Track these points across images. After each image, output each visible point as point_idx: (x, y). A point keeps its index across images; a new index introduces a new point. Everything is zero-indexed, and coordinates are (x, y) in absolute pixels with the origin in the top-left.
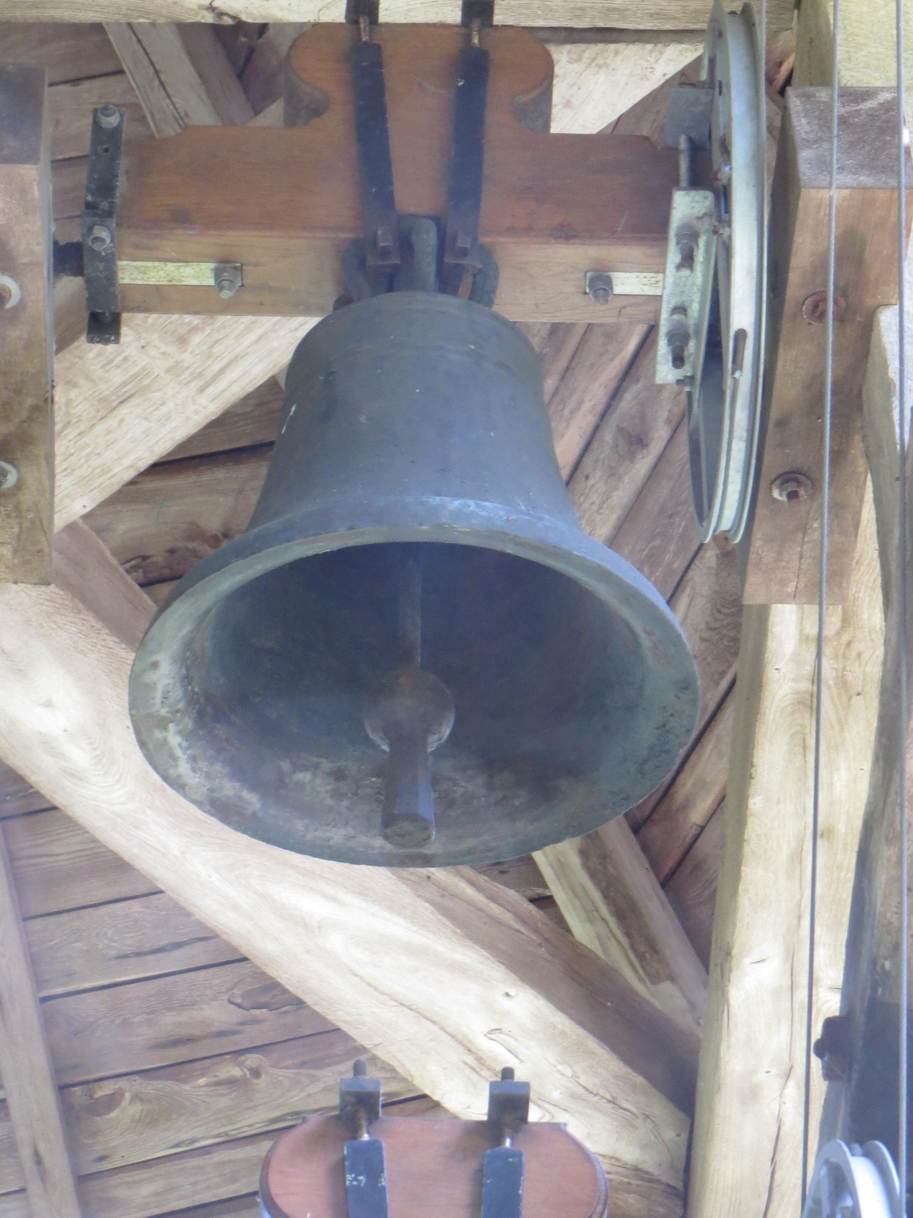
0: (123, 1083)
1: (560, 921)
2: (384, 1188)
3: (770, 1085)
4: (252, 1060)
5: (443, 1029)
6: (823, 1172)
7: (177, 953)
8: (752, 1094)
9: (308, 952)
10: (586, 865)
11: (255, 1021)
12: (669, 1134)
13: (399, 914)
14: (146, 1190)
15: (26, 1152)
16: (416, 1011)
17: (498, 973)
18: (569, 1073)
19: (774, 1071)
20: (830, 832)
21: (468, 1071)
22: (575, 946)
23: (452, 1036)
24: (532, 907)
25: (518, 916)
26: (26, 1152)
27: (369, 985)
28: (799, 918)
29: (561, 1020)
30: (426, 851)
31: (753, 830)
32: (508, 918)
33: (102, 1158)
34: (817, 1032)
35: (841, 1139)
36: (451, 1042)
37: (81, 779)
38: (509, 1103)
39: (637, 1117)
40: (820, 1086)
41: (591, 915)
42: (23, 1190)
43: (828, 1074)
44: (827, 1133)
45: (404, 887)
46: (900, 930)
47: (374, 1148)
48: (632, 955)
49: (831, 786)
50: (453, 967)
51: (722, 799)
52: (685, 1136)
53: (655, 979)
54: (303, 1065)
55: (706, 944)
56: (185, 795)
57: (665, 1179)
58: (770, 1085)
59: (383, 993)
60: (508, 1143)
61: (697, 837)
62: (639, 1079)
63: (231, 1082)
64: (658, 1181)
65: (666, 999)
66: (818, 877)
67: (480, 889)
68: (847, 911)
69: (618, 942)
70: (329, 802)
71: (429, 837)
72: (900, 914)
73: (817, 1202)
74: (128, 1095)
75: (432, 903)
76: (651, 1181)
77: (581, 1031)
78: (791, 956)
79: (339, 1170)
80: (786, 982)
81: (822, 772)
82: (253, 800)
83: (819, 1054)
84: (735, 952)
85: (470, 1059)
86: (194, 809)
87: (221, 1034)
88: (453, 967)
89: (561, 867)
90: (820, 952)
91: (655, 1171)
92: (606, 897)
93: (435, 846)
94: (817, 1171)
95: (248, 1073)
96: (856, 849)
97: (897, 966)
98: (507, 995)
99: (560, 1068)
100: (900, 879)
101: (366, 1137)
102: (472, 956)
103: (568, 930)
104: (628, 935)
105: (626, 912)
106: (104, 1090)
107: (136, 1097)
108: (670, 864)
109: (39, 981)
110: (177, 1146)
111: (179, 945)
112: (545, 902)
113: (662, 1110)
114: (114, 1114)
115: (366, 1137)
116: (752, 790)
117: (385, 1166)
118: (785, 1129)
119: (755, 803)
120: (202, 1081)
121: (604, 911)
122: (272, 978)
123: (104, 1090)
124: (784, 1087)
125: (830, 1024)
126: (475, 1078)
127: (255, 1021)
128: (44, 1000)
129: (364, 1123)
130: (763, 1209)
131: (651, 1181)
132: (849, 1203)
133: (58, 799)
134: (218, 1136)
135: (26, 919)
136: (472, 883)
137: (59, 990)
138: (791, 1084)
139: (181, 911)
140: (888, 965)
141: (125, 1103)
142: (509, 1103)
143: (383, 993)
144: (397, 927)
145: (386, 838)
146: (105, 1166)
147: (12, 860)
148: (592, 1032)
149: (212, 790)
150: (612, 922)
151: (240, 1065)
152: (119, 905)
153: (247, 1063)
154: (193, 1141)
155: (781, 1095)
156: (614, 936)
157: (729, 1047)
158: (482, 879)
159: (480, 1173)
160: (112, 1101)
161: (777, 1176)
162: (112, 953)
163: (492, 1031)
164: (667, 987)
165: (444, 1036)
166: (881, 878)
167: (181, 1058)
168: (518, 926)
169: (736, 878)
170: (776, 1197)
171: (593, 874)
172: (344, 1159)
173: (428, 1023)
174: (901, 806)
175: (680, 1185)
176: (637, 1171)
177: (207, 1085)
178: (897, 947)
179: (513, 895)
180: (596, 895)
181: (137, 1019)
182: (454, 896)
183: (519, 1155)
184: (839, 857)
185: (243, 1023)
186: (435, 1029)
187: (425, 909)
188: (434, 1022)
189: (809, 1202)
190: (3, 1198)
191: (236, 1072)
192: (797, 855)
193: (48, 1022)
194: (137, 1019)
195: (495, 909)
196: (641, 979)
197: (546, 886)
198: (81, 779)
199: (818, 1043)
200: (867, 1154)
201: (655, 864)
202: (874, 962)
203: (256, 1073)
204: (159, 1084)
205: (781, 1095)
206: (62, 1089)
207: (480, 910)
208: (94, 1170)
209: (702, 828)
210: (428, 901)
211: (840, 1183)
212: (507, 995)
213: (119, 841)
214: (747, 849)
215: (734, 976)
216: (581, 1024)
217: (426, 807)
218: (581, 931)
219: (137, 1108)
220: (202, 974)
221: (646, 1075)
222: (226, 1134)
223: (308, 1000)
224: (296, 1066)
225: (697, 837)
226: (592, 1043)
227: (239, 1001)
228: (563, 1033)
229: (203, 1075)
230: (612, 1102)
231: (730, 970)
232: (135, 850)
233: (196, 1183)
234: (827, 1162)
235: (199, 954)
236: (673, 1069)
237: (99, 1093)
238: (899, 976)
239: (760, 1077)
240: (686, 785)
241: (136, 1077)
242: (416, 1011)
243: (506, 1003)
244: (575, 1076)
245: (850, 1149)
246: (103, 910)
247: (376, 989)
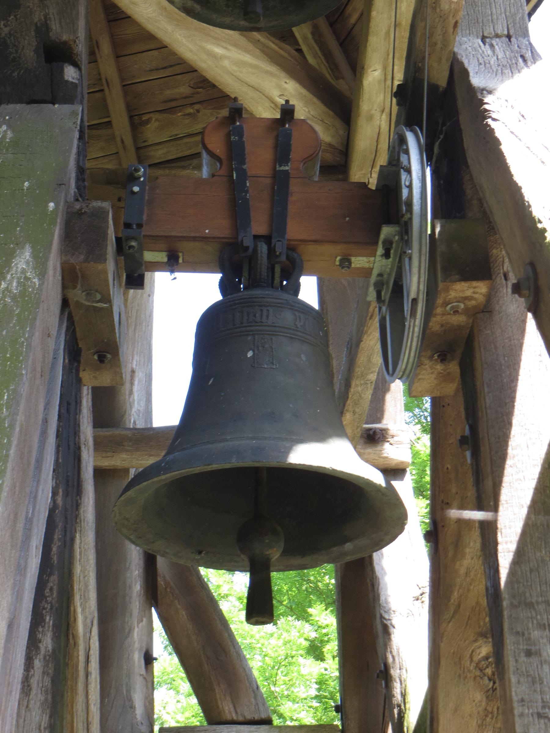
0: (152, 115)
1: (304, 57)
2: (244, 141)
3: (377, 115)
4: (197, 107)
5: (263, 94)
6: (396, 137)
7: (171, 69)
8: (370, 118)
9: (217, 67)
10: (314, 38)
11: (198, 93)
12: (341, 132)
13: (248, 53)
14: (161, 152)
15: (118, 139)
16: (254, 88)
17: (283, 74)
18: (307, 110)
19: (378, 110)
20: (400, 24)
21: (272, 109)
22: (310, 66)
23: (267, 97)
24: (294, 52)
25: (289, 54)
26: (118, 139)
27: (238, 79)
28: (388, 55)
29: (304, 91)
30: (258, 25)
31: (373, 24)
32: (286, 55)
33: (145, 141)
34: (395, 90)
35: (403, 125)
36: (266, 99)
37: (136, 5)
38: (288, 112)
39: (330, 126)
40: (395, 108)
41: (315, 56)
42: (117, 153)
43: (398, 104)
44: (397, 123)
45: (250, 44)
46: (425, 52)
47: (241, 127)
48: (329, 70)
49: (400, 8)
50: (267, 72)
51: (362, 14)
52: (347, 133)
53: (337, 78)
54: (215, 108)
55: (356, 68)
56: (174, 6)
57: (340, 148)
58: (377, 115)
59: (243, 82)
60: (287, 126)
61: (353, 28)
62: (331, 113)
63: (189, 114)
64: (337, 149)
65: (341, 85)
66: (396, 41)
67: (277, 45)
68: (407, 40)
69: (324, 65)
70: (224, 8)
71: (259, 20)
72: (425, 46)
73: (394, 148)
74: (154, 119)
75: (260, 50)
76: (335, 149)
77: (311, 96)
78: (385, 68)
79: (228, 135)
80: (383, 78)
81: (398, 3)
82: (198, 7)
83: (395, 97)
84: (366, 67)
85: (273, 105)
86: (176, 10)
87: (186, 98)
88: (267, 72)
89: (305, 38)
90: (395, 67)
91: (336, 145)
92: (320, 48)
93: (262, 23)
94: (394, 136)
95: (195, 111)
96: (409, 31)
97: (424, 65)
98: (286, 82)
99: (304, 108)
100: (425, 34)
101: (238, 123)
102: (273, 69)
103: (307, 61)
104: (328, 62)
105: (327, 54)
106: (145, 118)
107: (156, 120)
108: (343, 38)
109: (122, 79)
110: (171, 137)
111: (171, 66)
112: (300, 51)
113: (338, 123)
114: (149, 126)
115: (238, 123)
116: (373, 9)
117: (245, 133)
118: (382, 130)
119: (374, 14)
120: (179, 114)
121: (320, 54)
122: (205, 77)
123: (145, 118)
124: (381, 115)
125: (399, 86)
126: (274, 112)
127: (198, 93)
128: (124, 86)
129: (237, 119)
130: (373, 158)
131: (335, 149)
132: (405, 147)
133: (129, 12)
134: (185, 133)
135: (117, 57)
136: (274, 43)
137: (130, 82)
138: (384, 114)
139: (173, 53)
140: (420, 65)
141: (153, 122)
142: (288, 112)
143: (243, 82)
144: (247, 58)
145: (245, 20)
146: (146, 144)
147: (112, 36)
148: (315, 96)
149: (183, 4)
150: (323, 58)
151: (193, 108)
152: (150, 52)
153: (195, 108)
154: (176, 135)
155: (380, 118)
156: (323, 63)
157: (363, 101)
158: (277, 41)
159: (277, 137)
160: (148, 121)
161: (379, 147)
162: (148, 69)
163: (280, 95)
164: (341, 81)
165: (264, 97)
166: (419, 34)
167: (171, 108)
168: (290, 58)
169: (367, 40)
170: (378, 154)
171: (316, 41)
172: (230, 131)
173: (258, 92)
174: (427, 6)
175: (344, 150)
176: (330, 145)
177: (181, 116)
178: (424, 58)
179: (288, 47)
180: (317, 48)
181: (157, 92)
182: (267, 47)
183: (291, 130)
184: (403, 34)
185: (193, 94)
186: (260, 94)
187: (257, 52)
188: (260, 92)
189: (391, 148)
190: (90, 732)
191: (191, 111)
192: (388, 33)
193: (126, 94)
194: (157, 92)
195: (282, 52)
196: (332, 78)
197: (299, 45)
198: (136, 5)
199: (395, 93)
200: (412, 130)
201: (338, 38)
202: (415, 64)
203: (198, 111)
204: (165, 115)
205: (380, 118)
206: (131, 117)
207: (277, 52)
208: (142, 145)
209: (354, 25)
210: (258, 49)
211: (402, 140)
212: (286, 82)
213: (151, 27)
214: (371, 30)
215: (365, 76)
216: (311, 93)
217: (259, 9)
218: (311, 60)
219: (157, 124)
220: (179, 76)
221: (333, 111)
222: (188, 133)
223: (217, 84)
224: (212, 109)
225: (353, 28)
226: (315, 100)
227: (192, 86)
228: (305, 96)
229: (180, 112)
230: (322, 121)
231: (364, 74)
232: (156, 30)
233: (177, 150)
234: (397, 133)
235: (178, 69)
236: (342, 107)
237: (144, 119)
238: (424, 69)
239: (373, 112)
240: (349, 9)
241: (156, 113)
242: (254, 88)
243: (286, 86)
244: (309, 112)
245: (406, 129)
246: (144, 54)
247: (240, 80)
